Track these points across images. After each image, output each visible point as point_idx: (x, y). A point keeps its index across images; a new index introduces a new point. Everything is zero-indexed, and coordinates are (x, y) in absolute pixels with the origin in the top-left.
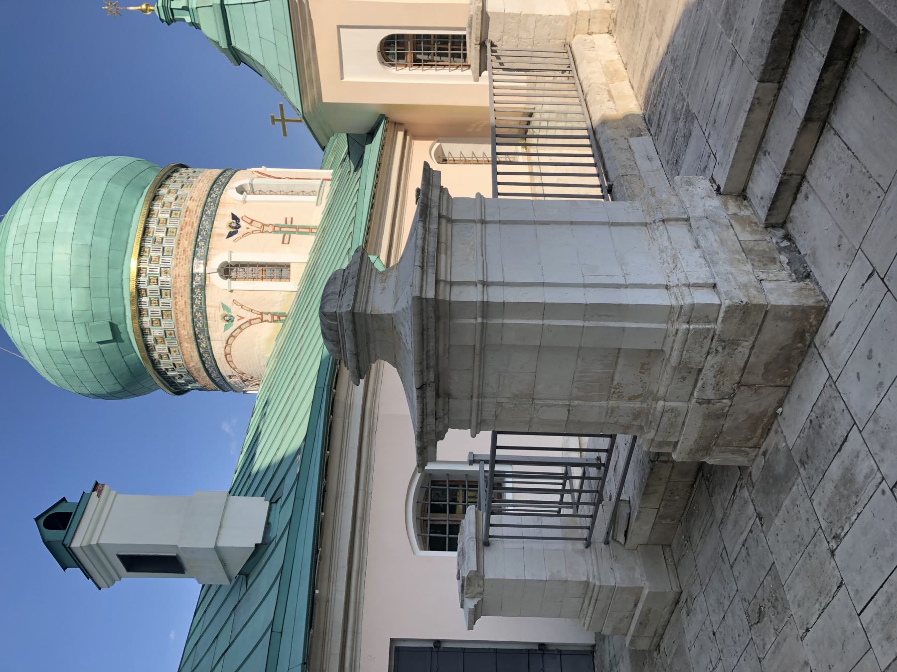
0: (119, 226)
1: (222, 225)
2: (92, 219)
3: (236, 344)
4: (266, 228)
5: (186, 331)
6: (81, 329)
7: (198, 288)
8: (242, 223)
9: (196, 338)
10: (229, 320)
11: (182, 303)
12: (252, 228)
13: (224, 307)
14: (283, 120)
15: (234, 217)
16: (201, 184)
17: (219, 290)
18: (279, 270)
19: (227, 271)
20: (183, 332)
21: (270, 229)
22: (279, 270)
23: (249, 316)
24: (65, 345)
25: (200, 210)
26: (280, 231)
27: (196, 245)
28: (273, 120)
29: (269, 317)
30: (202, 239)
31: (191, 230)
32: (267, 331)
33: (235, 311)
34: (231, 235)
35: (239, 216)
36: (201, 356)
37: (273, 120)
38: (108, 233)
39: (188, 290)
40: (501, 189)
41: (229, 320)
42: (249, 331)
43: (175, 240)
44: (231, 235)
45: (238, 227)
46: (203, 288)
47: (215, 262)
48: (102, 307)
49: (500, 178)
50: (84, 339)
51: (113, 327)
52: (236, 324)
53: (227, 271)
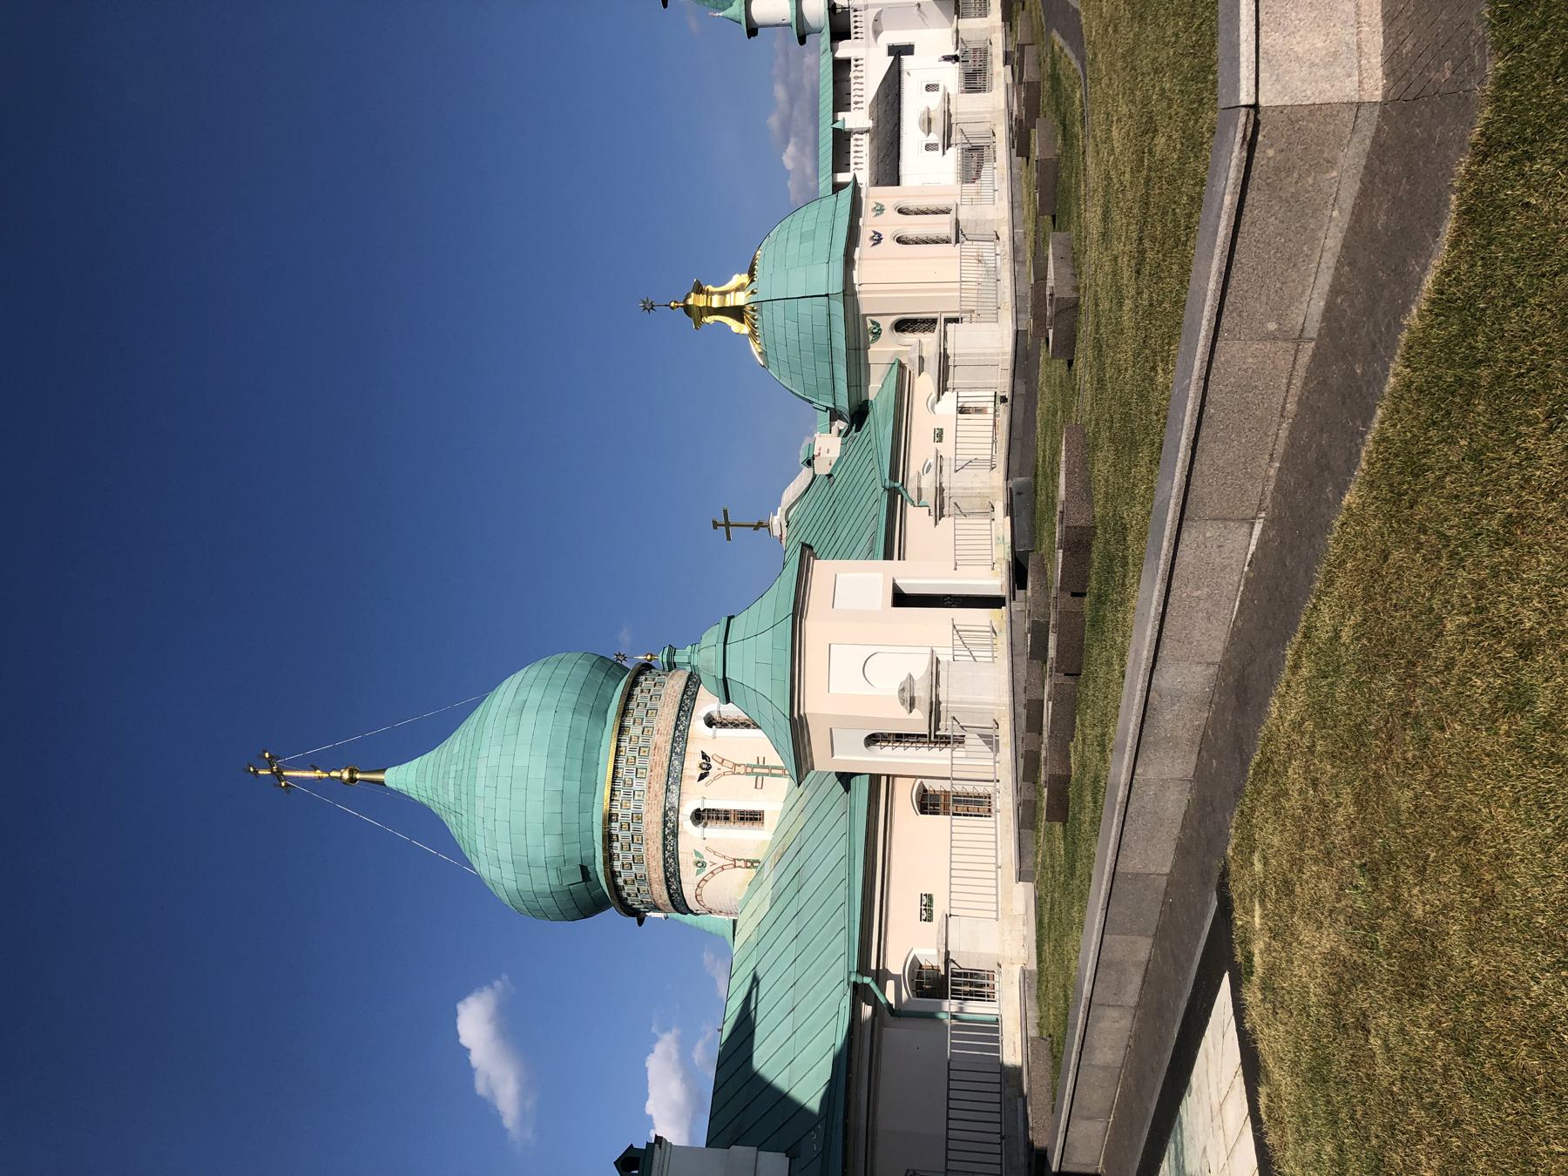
0: (589, 764)
1: (692, 765)
2: (562, 761)
3: (707, 887)
4: (738, 769)
5: (657, 874)
6: (553, 874)
7: (670, 833)
8: (712, 763)
9: (667, 880)
10: (701, 865)
11: (653, 852)
12: (724, 769)
13: (697, 853)
14: (727, 525)
15: (704, 756)
16: (666, 710)
17: (691, 837)
18: (754, 817)
19: (698, 817)
20: (654, 876)
21: (741, 770)
22: (754, 817)
23: (722, 862)
24: (535, 887)
25: (669, 747)
26: (752, 773)
27: (668, 790)
28: (715, 525)
29: (742, 863)
30: (673, 778)
31: (662, 772)
32: (743, 875)
33: (707, 858)
34: (702, 777)
35: (709, 754)
36: (670, 896)
37: (715, 525)
38: (577, 775)
39: (660, 835)
40: (951, 1166)
41: (701, 865)
42: (720, 876)
43: (645, 783)
44: (702, 777)
45: (709, 767)
46: (676, 835)
47: (687, 811)
48: (574, 852)
49: (952, 1124)
50: (555, 881)
51: (584, 870)
52: (708, 869)
53: (698, 817)
